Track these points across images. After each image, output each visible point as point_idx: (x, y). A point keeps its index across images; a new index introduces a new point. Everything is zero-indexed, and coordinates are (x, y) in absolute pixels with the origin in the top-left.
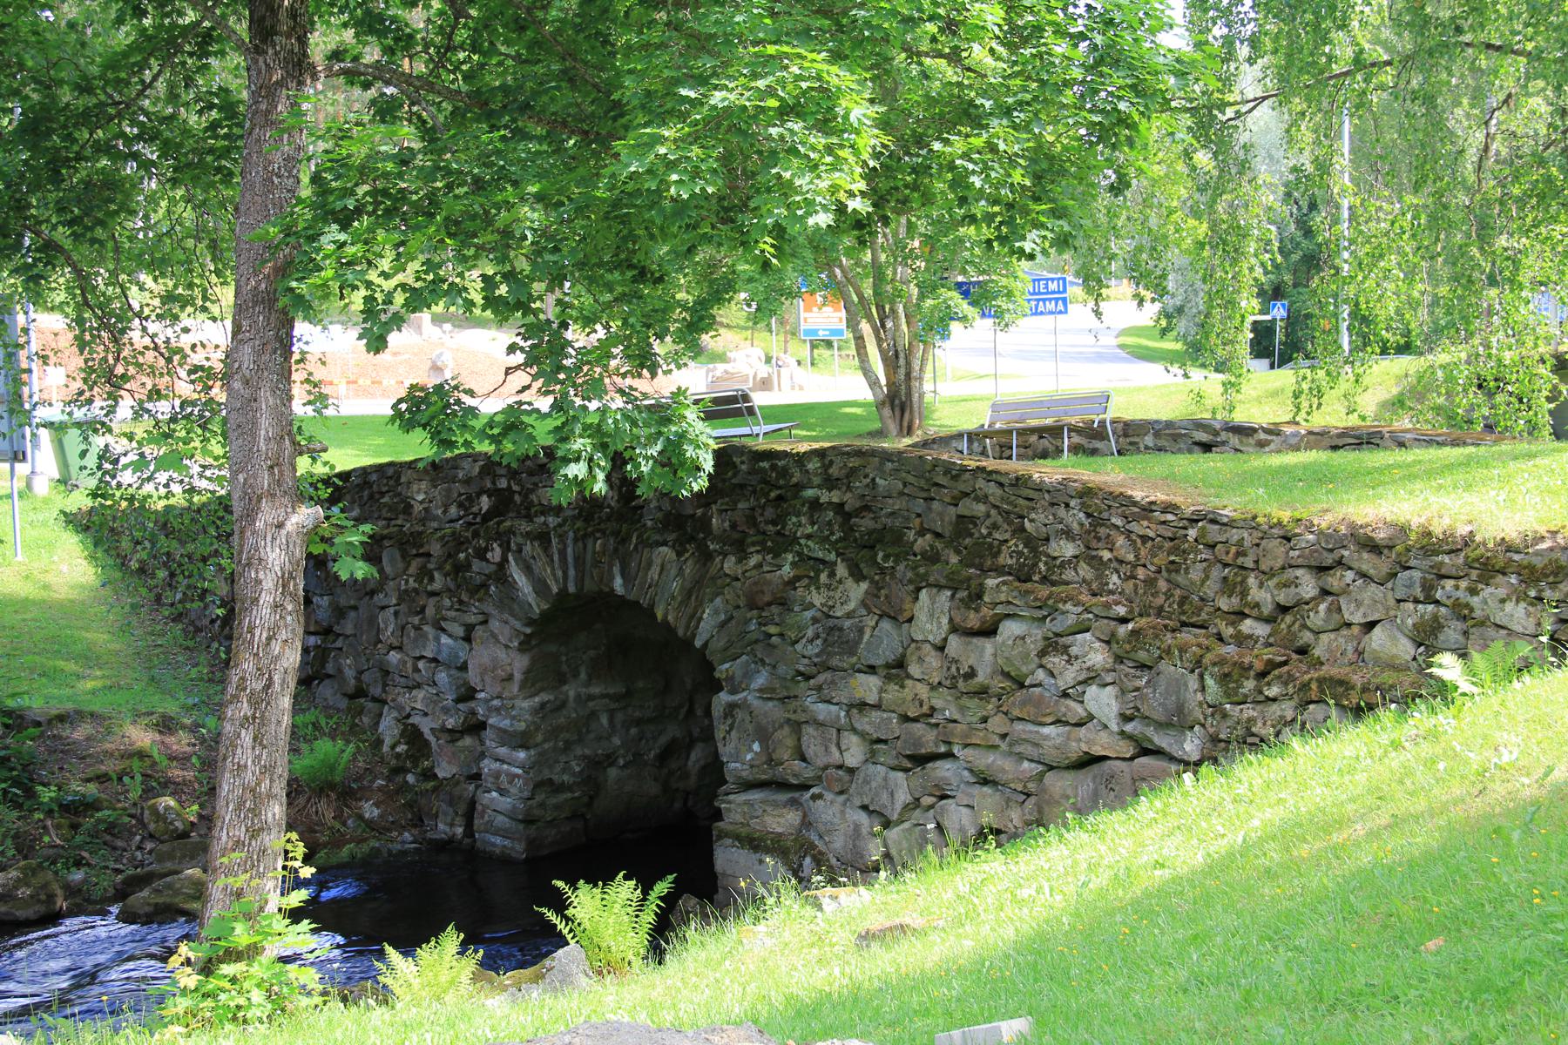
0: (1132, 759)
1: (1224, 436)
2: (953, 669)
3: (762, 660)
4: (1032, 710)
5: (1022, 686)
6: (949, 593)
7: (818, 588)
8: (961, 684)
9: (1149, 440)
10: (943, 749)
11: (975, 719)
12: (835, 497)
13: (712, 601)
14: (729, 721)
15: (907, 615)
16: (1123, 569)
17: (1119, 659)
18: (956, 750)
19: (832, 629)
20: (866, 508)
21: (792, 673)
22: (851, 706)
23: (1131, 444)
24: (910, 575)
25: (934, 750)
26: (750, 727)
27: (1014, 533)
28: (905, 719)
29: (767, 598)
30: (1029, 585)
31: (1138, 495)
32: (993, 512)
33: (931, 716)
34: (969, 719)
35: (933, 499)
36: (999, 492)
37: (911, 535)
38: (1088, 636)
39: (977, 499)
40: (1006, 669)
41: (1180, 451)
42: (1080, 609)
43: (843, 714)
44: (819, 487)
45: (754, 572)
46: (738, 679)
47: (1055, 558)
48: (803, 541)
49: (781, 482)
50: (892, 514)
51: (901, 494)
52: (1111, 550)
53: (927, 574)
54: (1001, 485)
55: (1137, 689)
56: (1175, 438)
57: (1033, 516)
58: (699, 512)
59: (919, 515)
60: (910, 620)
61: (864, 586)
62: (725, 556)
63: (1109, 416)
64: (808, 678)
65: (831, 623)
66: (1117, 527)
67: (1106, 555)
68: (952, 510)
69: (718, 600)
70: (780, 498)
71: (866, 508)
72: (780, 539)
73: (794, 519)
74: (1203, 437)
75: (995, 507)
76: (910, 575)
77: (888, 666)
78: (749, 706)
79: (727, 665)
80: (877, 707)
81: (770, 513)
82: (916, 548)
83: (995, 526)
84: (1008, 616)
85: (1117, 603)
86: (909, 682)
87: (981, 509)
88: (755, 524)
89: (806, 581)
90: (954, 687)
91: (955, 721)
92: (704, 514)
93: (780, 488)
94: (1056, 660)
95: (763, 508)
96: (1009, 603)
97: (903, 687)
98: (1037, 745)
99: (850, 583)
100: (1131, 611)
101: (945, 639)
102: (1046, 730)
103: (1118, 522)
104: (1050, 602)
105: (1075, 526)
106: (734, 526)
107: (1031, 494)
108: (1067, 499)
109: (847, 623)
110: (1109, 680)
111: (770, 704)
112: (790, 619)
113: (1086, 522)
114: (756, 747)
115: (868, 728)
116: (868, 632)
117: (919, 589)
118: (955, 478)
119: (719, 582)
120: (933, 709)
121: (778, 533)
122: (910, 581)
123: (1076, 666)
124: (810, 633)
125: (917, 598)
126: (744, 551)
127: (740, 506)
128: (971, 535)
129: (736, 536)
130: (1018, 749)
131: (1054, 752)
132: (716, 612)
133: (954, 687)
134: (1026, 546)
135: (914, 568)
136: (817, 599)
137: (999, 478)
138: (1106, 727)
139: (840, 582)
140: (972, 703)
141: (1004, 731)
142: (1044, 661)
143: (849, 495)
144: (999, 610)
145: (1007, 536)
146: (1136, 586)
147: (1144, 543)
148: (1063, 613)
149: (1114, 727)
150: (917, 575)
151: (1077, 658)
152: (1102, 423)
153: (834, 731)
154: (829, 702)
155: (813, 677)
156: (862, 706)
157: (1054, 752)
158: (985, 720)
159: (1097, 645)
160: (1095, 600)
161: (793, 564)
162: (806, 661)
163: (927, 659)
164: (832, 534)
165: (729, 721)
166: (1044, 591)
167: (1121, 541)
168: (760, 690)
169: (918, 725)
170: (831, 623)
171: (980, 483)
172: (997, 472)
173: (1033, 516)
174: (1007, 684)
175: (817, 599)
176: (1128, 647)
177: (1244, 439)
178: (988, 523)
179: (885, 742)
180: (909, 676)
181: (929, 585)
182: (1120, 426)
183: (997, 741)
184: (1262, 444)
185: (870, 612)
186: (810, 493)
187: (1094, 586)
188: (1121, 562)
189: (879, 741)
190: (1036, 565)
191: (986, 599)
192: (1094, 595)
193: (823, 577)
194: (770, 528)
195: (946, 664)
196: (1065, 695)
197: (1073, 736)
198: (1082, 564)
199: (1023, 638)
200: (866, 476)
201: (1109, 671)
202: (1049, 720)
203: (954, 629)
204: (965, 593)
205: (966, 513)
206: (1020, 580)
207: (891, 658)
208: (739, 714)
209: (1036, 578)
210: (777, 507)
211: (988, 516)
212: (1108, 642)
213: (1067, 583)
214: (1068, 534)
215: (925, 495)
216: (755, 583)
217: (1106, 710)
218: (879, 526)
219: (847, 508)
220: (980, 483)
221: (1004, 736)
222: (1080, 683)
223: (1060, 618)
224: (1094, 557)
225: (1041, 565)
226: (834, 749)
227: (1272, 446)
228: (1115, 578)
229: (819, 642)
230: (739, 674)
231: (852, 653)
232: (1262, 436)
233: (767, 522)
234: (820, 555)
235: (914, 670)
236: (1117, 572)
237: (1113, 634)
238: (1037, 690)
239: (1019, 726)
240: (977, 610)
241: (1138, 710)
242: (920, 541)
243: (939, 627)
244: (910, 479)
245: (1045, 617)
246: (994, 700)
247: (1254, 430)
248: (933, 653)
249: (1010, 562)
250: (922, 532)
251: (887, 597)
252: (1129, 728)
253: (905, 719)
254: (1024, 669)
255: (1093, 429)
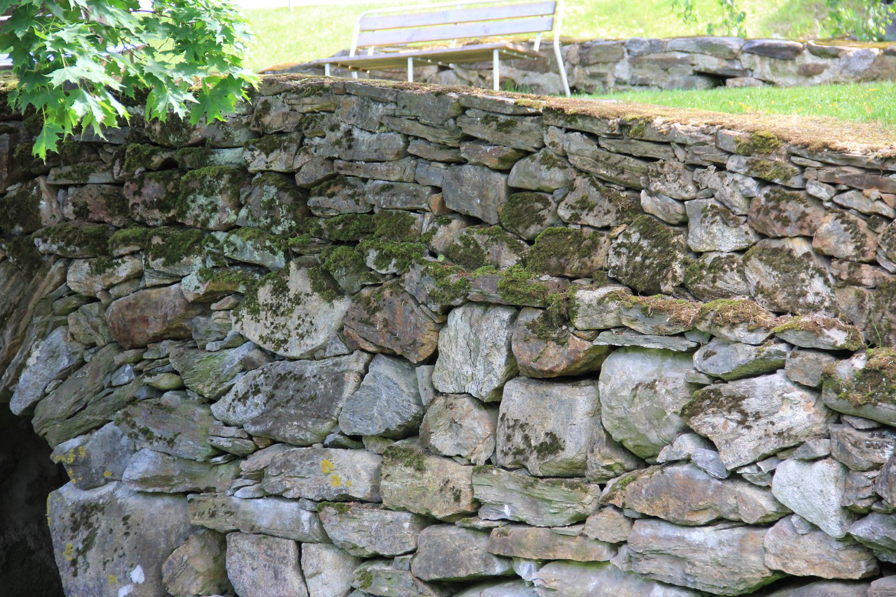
0: (867, 580)
1: (746, 60)
2: (518, 439)
3: (146, 432)
4: (673, 504)
5: (642, 462)
6: (506, 315)
7: (255, 312)
8: (533, 462)
9: (623, 70)
10: (498, 569)
11: (560, 520)
12: (279, 162)
13: (43, 336)
14: (83, 534)
15: (426, 352)
16: (832, 269)
17: (836, 416)
18: (523, 570)
19: (283, 378)
20: (334, 179)
21: (204, 452)
22: (322, 502)
23: (593, 76)
24: (430, 286)
25: (483, 571)
26: (126, 544)
27: (622, 213)
28: (426, 520)
29: (155, 328)
30: (655, 300)
31: (856, 148)
32: (580, 182)
33: (475, 514)
34: (549, 520)
35: (462, 162)
36: (590, 148)
37: (424, 223)
38: (777, 379)
39: (549, 162)
40: (617, 436)
41: (672, 85)
42: (761, 336)
43: (306, 516)
44: (246, 145)
45: (125, 288)
46: (96, 464)
47: (699, 254)
48: (220, 236)
49: (172, 139)
50: (385, 189)
51: (404, 154)
52: (809, 239)
53: (465, 285)
54: (593, 136)
55: (877, 466)
56: (666, 66)
57: (657, 185)
58: (13, 190)
59: (437, 190)
60: (432, 360)
61: (342, 306)
62: (69, 261)
63: (556, 36)
64: (234, 458)
65: (280, 368)
66: (819, 201)
67: (800, 247)
68: (500, 178)
69: (57, 336)
70: (169, 164)
71: (334, 179)
72: (177, 233)
73: (202, 200)
74: (712, 63)
75: (580, 172)
76: (430, 286)
77: (387, 436)
78: (121, 507)
79: (74, 442)
80: (375, 502)
81: (152, 189)
82: (437, 243)
83: (585, 205)
84: (613, 349)
85: (830, 326)
86: (432, 462)
87: (554, 177)
88: (123, 209)
89: (231, 300)
90: (520, 466)
91: (522, 523)
92: (23, 194)
93: (171, 148)
94: (719, 420)
95: (141, 182)
96: (622, 328)
97: (420, 469)
98: (677, 559)
99: (315, 302)
100: (854, 339)
101: (499, 390)
102: (697, 536)
103: (823, 192)
104: (702, 326)
105: (738, 202)
106: (82, 212)
107: (652, 150)
108: (719, 157)
109: (311, 368)
110: (821, 451)
111: (159, 503)
112: (200, 362)
113: (760, 194)
114: (137, 575)
115: (355, 538)
116: (351, 381)
117: (447, 310)
118: (506, 127)
119: (59, 305)
120: (478, 504)
121: (171, 223)
122: (432, 297)
123: (758, 429)
124: (240, 384)
125: (444, 324)
126: (105, 253)
127: (94, 178)
128: (540, 220)
129: (89, 228)
130: (645, 567)
131: (714, 571)
132: (53, 355)
133: (520, 466)
134: (644, 235)
135: (438, 276)
136: (254, 330)
137: (589, 126)
138: (814, 528)
139: (297, 300)
140: (557, 493)
141: (617, 537)
142: (695, 423)
143: (302, 159)
144: (604, 340)
145: (609, 220)
146: (861, 297)
147: (873, 226)
148: (727, 342)
149: (834, 527)
150: (446, 287)
151: (757, 416)
152: (547, 46)
153: (292, 546)
154: (279, 496)
155: (245, 457)
156: (344, 501)
157: (714, 571)
158: (581, 520)
159: (797, 394)
160: (787, 321)
161: (204, 274)
162: (232, 431)
163: (467, 423)
164: (277, 222)
165: (83, 534)
166: (689, 309)
167: (827, 224)
168: (143, 481)
169: (452, 531)
170: (280, 368)
171: (554, 135)
172: (584, 116)
173: (657, 185)
174: (618, 459)
175: (254, 330)
176: (858, 397)
177: (780, 65)
178: (571, 199)
179: (389, 559)
180: (430, 451)
181: (468, 302)
182: (575, 49)
183: (605, 554)
184: (808, 73)
185: (353, 348)
186: (227, 156)
187: (780, 298)
188: (829, 258)
189: (376, 557)
190: (666, 266)
191: (579, 323)
192: (779, 314)
193: (264, 294)
194: (157, 213)
195: (502, 432)
196: (734, 476)
197: (749, 545)
198: (755, 262)
199: (651, 386)
200: (334, 128)
201: (818, 436)
202: (703, 518)
203: (514, 372)
204: (537, 315)
205: (527, 184)
206: (635, 292)
207: (395, 422)
208: (102, 523)
209: (668, 287)
210: (166, 180)
211: (570, 187)
212: (816, 390)
213: (726, 295)
214: (726, 214)
215: (448, 155)
216: (129, 306)
217: (818, 501)
218: (362, 209)
219: (300, 180)
220: (554, 135)
221: (615, 547)
222: (765, 457)
223: (722, 351)
224: (776, 252)
225: (677, 267)
226: (291, 575)
227: (826, 75)
228: (817, 284)
229: (259, 399)
230: (97, 456)
231: (320, 417)
232: (809, 59)
233: (149, 206)
234: (257, 258)
235: (442, 441)
236: (822, 274)
237: (827, 376)
238: (681, 470)
239: (645, 530)
240: (561, 342)
241: (879, 499)
242: (442, 231)
243: (489, 370)
244: (417, 129)
245: (691, 351)
246: (594, 487)
247: (797, 51)
248: (477, 413)
249: (614, 261)
250: (445, 215)
251: (386, 324)
252: (861, 530)
253: (426, 520)
254: (653, 436)
255: (532, 55)
